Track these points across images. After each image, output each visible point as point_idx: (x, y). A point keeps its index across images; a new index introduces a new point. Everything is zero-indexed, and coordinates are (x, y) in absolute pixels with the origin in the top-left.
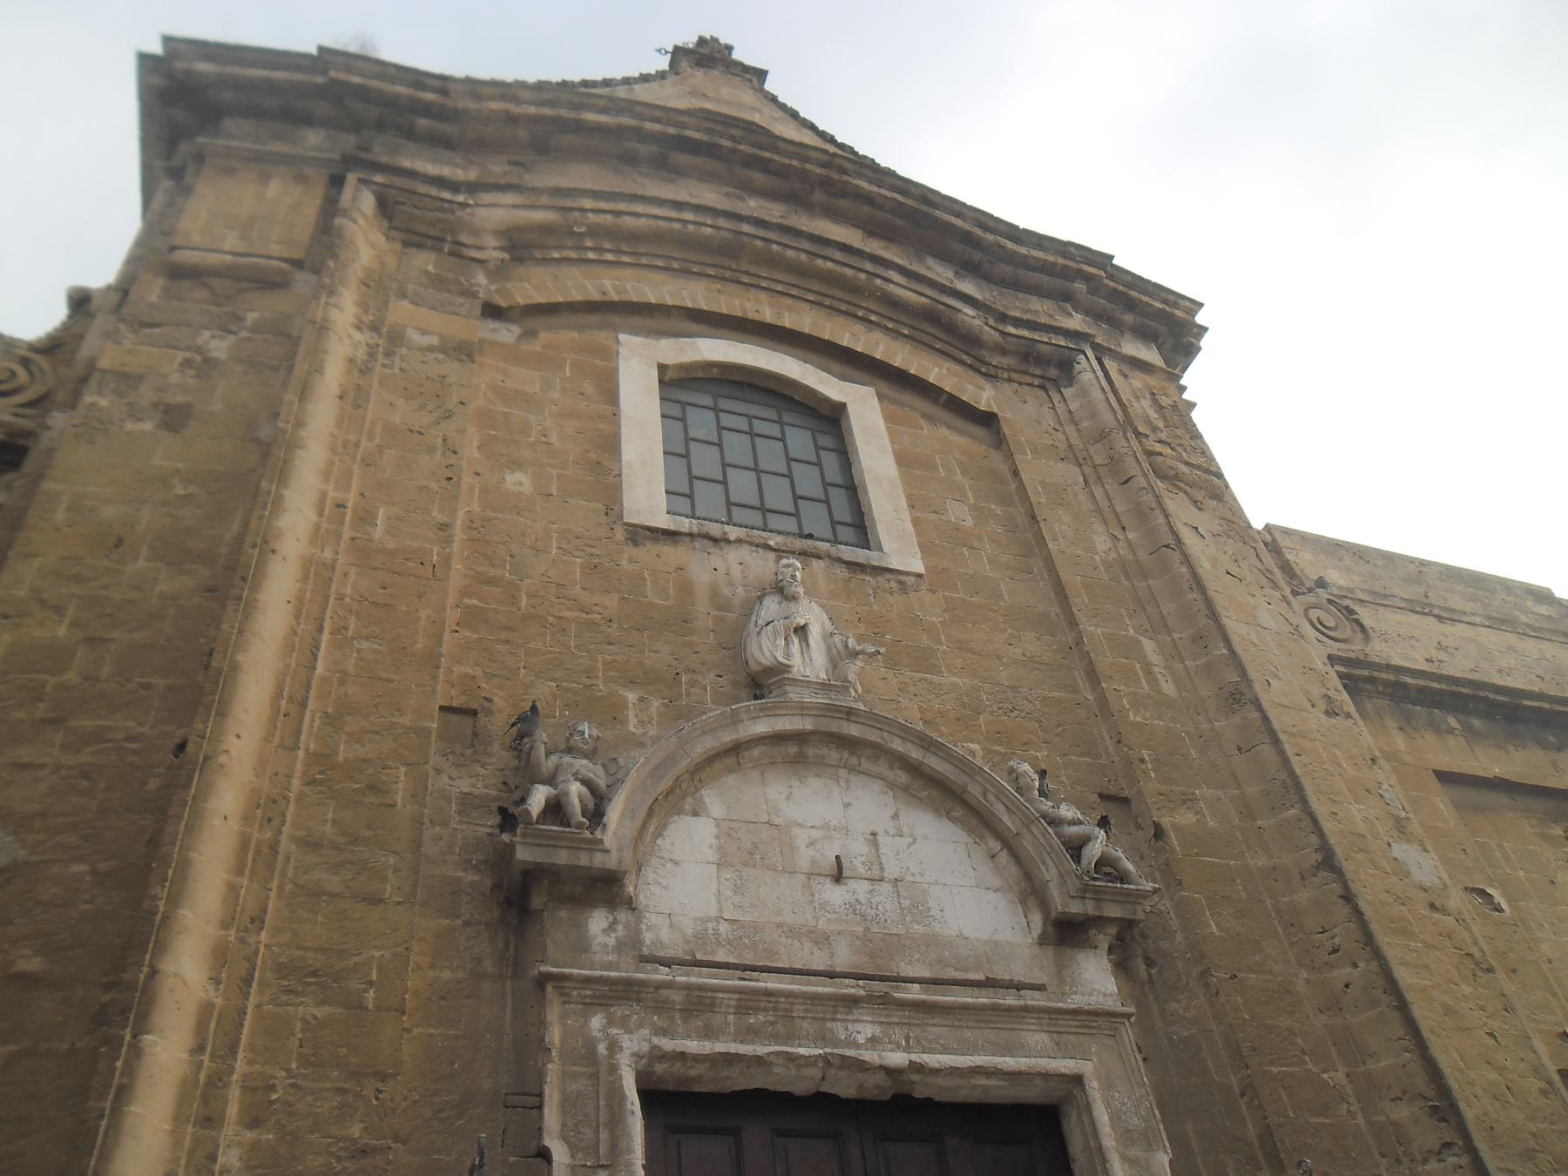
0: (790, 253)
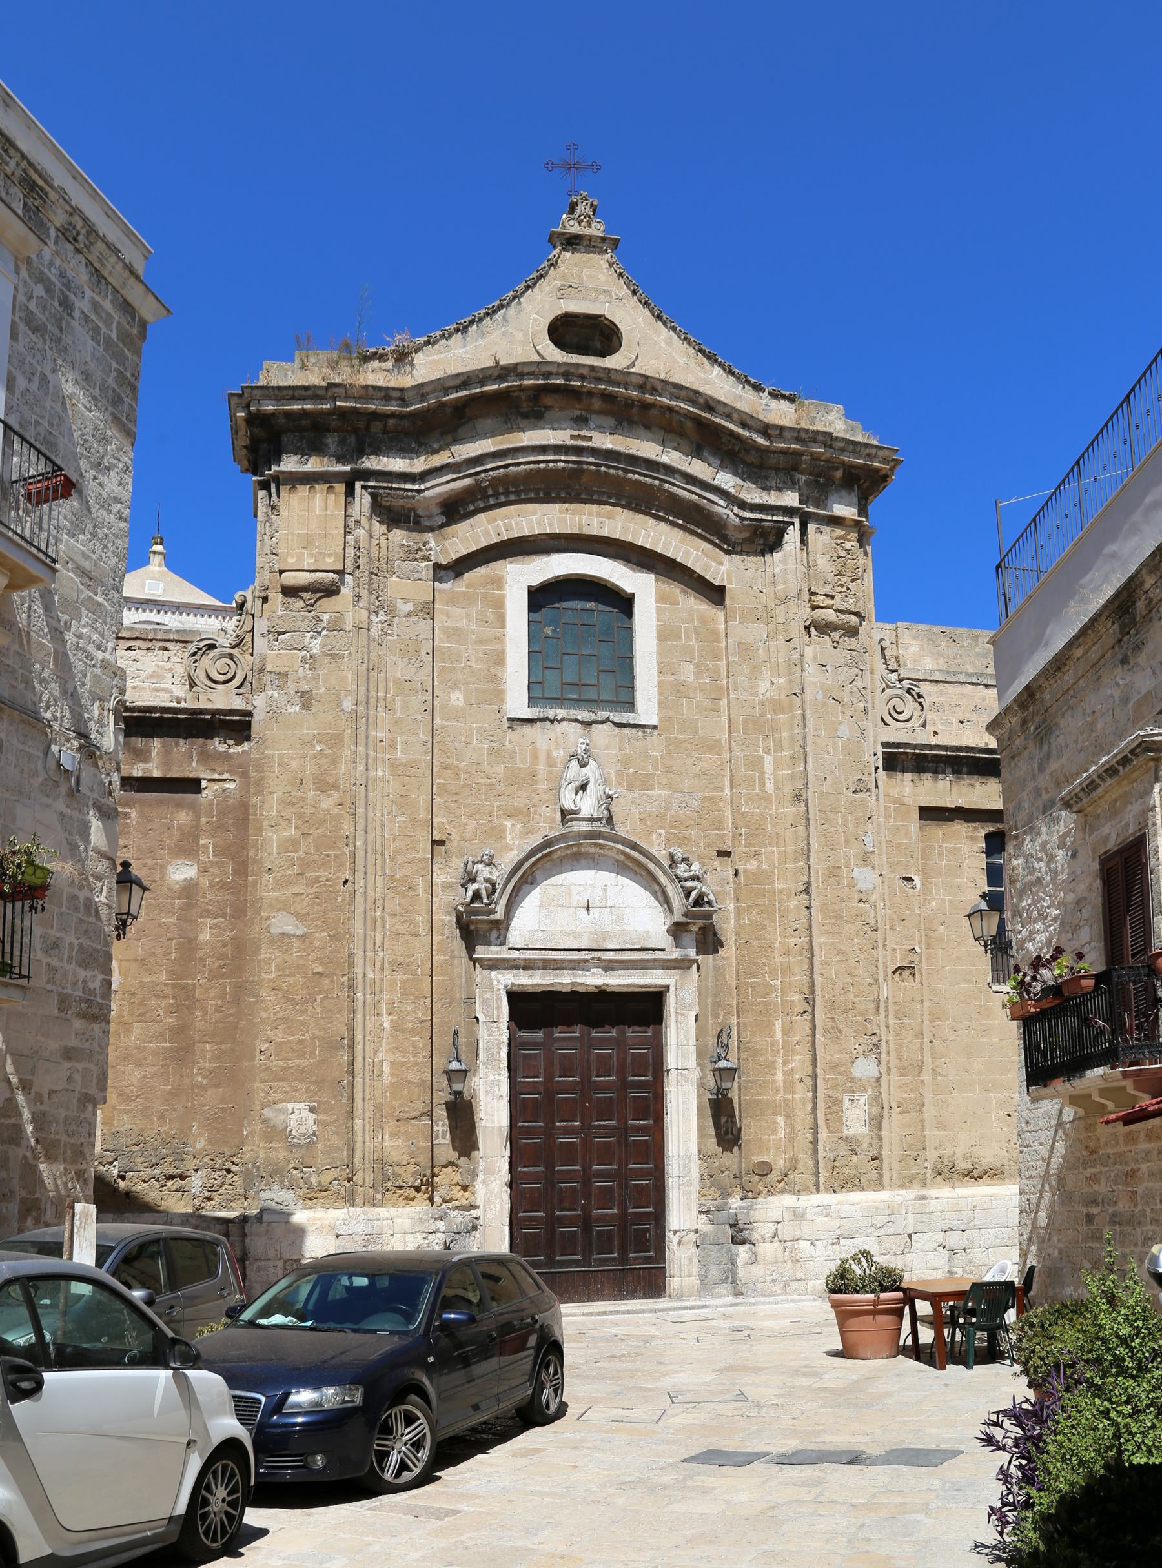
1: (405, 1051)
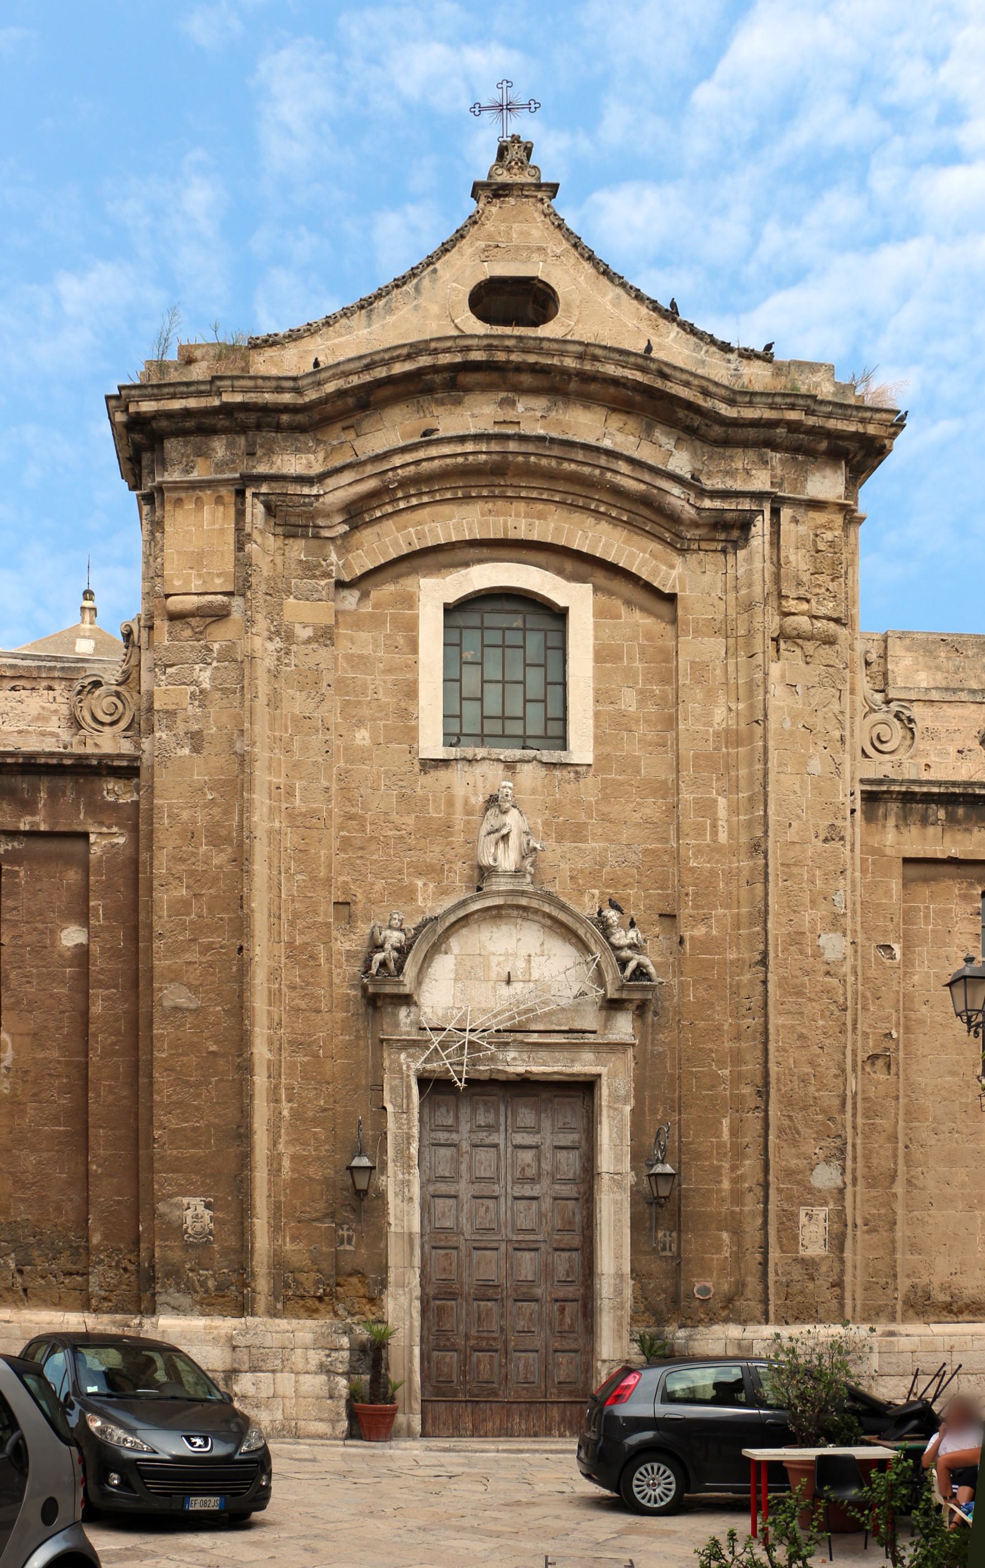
0: (544, 462)
1: (306, 1144)
